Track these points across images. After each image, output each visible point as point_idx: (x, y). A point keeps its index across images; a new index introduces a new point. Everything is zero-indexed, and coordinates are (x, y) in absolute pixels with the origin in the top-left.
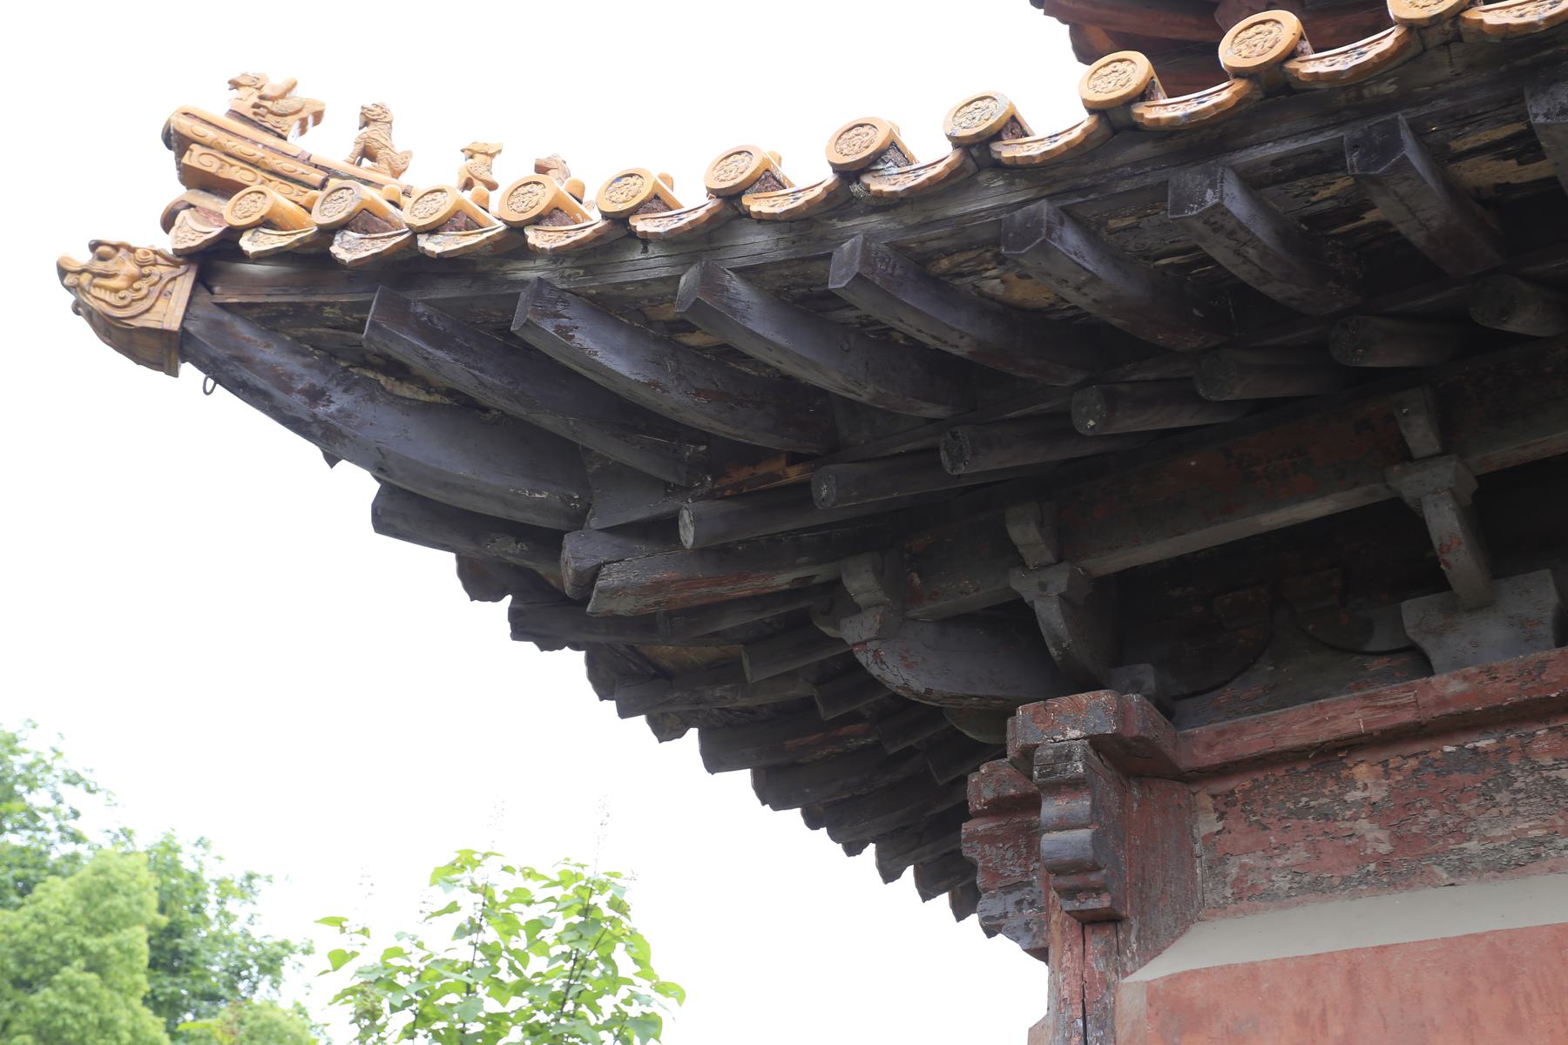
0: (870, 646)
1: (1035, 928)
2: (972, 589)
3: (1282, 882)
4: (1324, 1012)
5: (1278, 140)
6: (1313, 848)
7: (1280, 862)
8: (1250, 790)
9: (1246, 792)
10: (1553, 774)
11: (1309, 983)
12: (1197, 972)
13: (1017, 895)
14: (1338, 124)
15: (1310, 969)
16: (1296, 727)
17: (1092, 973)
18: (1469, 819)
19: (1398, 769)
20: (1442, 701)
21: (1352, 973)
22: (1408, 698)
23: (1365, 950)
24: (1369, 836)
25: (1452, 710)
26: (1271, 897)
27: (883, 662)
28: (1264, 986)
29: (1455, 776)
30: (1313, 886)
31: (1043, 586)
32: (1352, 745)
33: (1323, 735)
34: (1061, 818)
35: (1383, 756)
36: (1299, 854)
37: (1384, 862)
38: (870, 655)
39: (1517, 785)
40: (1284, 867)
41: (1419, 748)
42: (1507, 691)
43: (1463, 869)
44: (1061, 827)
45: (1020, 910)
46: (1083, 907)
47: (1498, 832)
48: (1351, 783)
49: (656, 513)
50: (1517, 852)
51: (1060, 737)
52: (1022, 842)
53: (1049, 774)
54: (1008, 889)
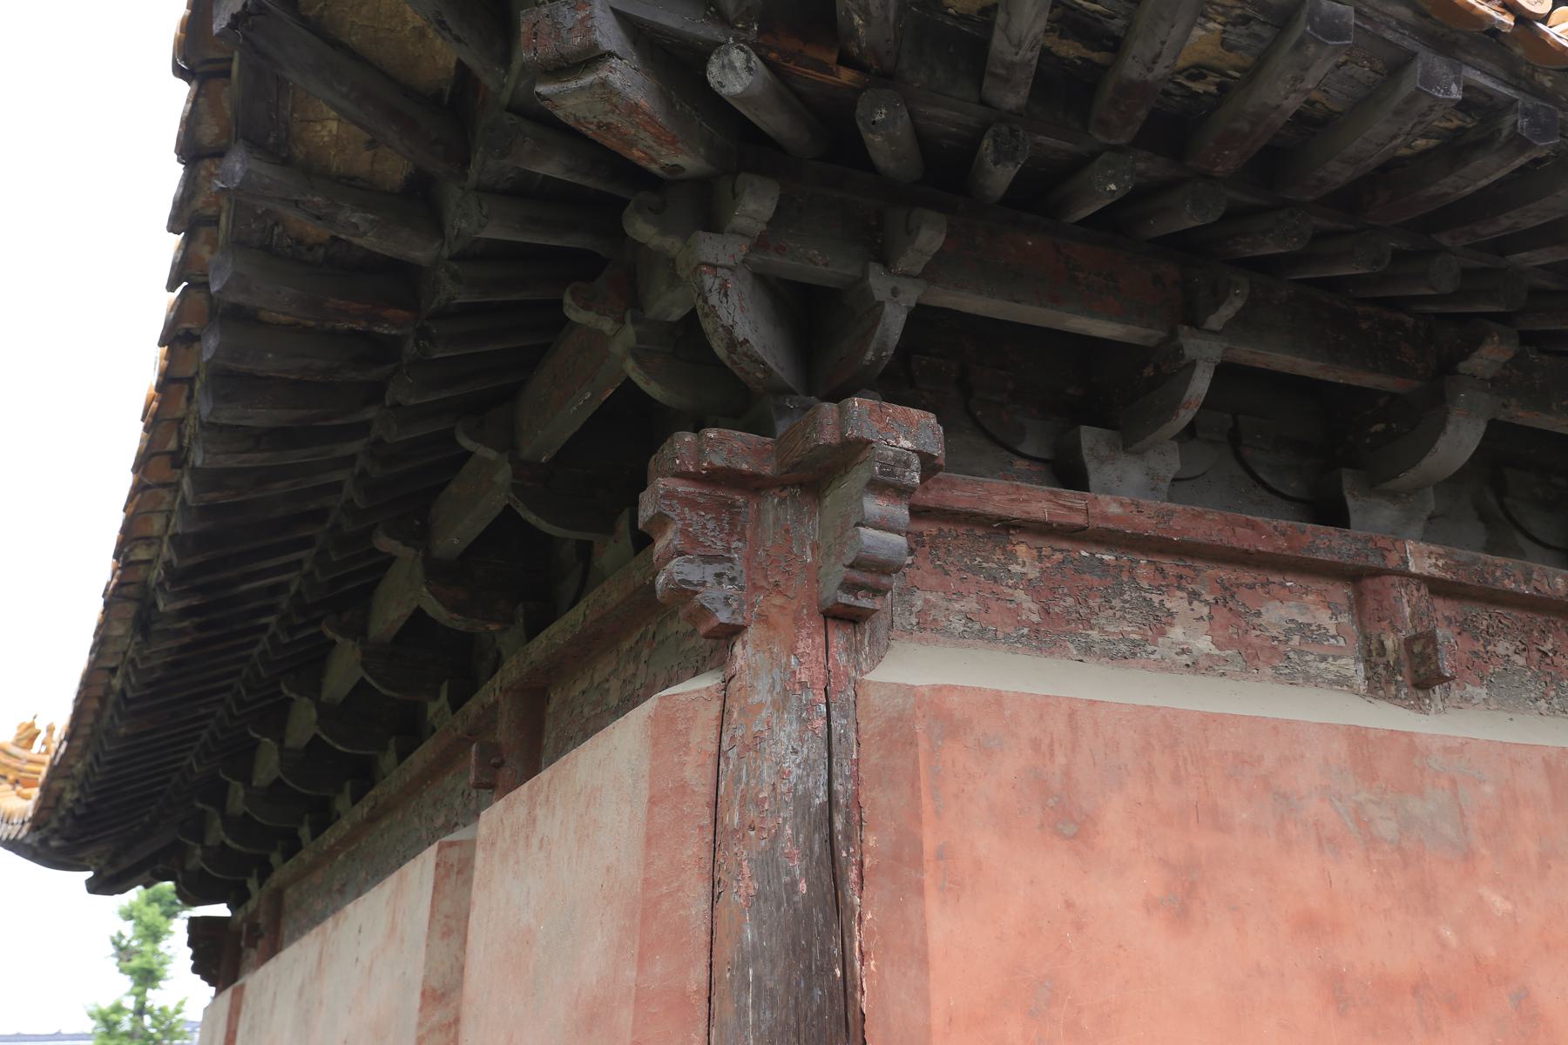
0: (720, 272)
1: (735, 605)
2: (817, 261)
3: (958, 625)
4: (1051, 745)
5: (1485, 73)
6: (983, 602)
7: (957, 606)
8: (936, 537)
9: (933, 538)
10: (1148, 596)
11: (1041, 717)
12: (954, 688)
13: (717, 568)
14: (1517, 88)
15: (1044, 705)
16: (996, 498)
17: (837, 665)
18: (1092, 612)
19: (1048, 557)
20: (1105, 517)
21: (1072, 715)
22: (1081, 505)
23: (1080, 700)
24: (1025, 605)
25: (1111, 526)
26: (946, 632)
27: (726, 295)
28: (1007, 713)
29: (1087, 576)
30: (981, 633)
31: (895, 292)
32: (1006, 527)
33: (1016, 512)
34: (882, 518)
35: (1040, 543)
36: (970, 604)
37: (1036, 630)
38: (717, 282)
39: (1126, 597)
40: (960, 612)
41: (1065, 545)
42: (1146, 523)
43: (1088, 649)
44: (876, 527)
45: (720, 583)
46: (857, 603)
47: (1111, 629)
48: (1012, 557)
49: (688, 29)
50: (1123, 647)
51: (893, 442)
52: (725, 516)
53: (888, 474)
54: (708, 559)
